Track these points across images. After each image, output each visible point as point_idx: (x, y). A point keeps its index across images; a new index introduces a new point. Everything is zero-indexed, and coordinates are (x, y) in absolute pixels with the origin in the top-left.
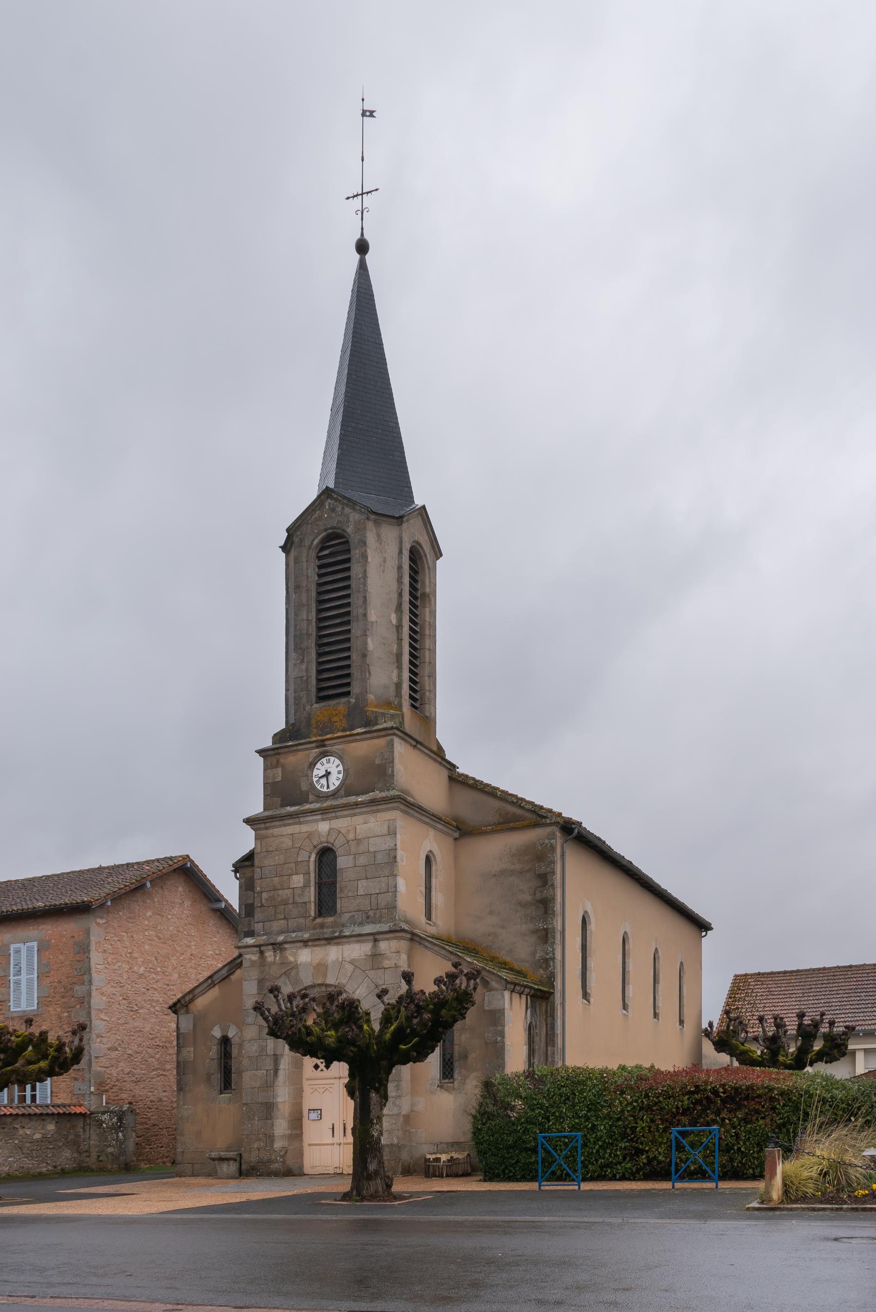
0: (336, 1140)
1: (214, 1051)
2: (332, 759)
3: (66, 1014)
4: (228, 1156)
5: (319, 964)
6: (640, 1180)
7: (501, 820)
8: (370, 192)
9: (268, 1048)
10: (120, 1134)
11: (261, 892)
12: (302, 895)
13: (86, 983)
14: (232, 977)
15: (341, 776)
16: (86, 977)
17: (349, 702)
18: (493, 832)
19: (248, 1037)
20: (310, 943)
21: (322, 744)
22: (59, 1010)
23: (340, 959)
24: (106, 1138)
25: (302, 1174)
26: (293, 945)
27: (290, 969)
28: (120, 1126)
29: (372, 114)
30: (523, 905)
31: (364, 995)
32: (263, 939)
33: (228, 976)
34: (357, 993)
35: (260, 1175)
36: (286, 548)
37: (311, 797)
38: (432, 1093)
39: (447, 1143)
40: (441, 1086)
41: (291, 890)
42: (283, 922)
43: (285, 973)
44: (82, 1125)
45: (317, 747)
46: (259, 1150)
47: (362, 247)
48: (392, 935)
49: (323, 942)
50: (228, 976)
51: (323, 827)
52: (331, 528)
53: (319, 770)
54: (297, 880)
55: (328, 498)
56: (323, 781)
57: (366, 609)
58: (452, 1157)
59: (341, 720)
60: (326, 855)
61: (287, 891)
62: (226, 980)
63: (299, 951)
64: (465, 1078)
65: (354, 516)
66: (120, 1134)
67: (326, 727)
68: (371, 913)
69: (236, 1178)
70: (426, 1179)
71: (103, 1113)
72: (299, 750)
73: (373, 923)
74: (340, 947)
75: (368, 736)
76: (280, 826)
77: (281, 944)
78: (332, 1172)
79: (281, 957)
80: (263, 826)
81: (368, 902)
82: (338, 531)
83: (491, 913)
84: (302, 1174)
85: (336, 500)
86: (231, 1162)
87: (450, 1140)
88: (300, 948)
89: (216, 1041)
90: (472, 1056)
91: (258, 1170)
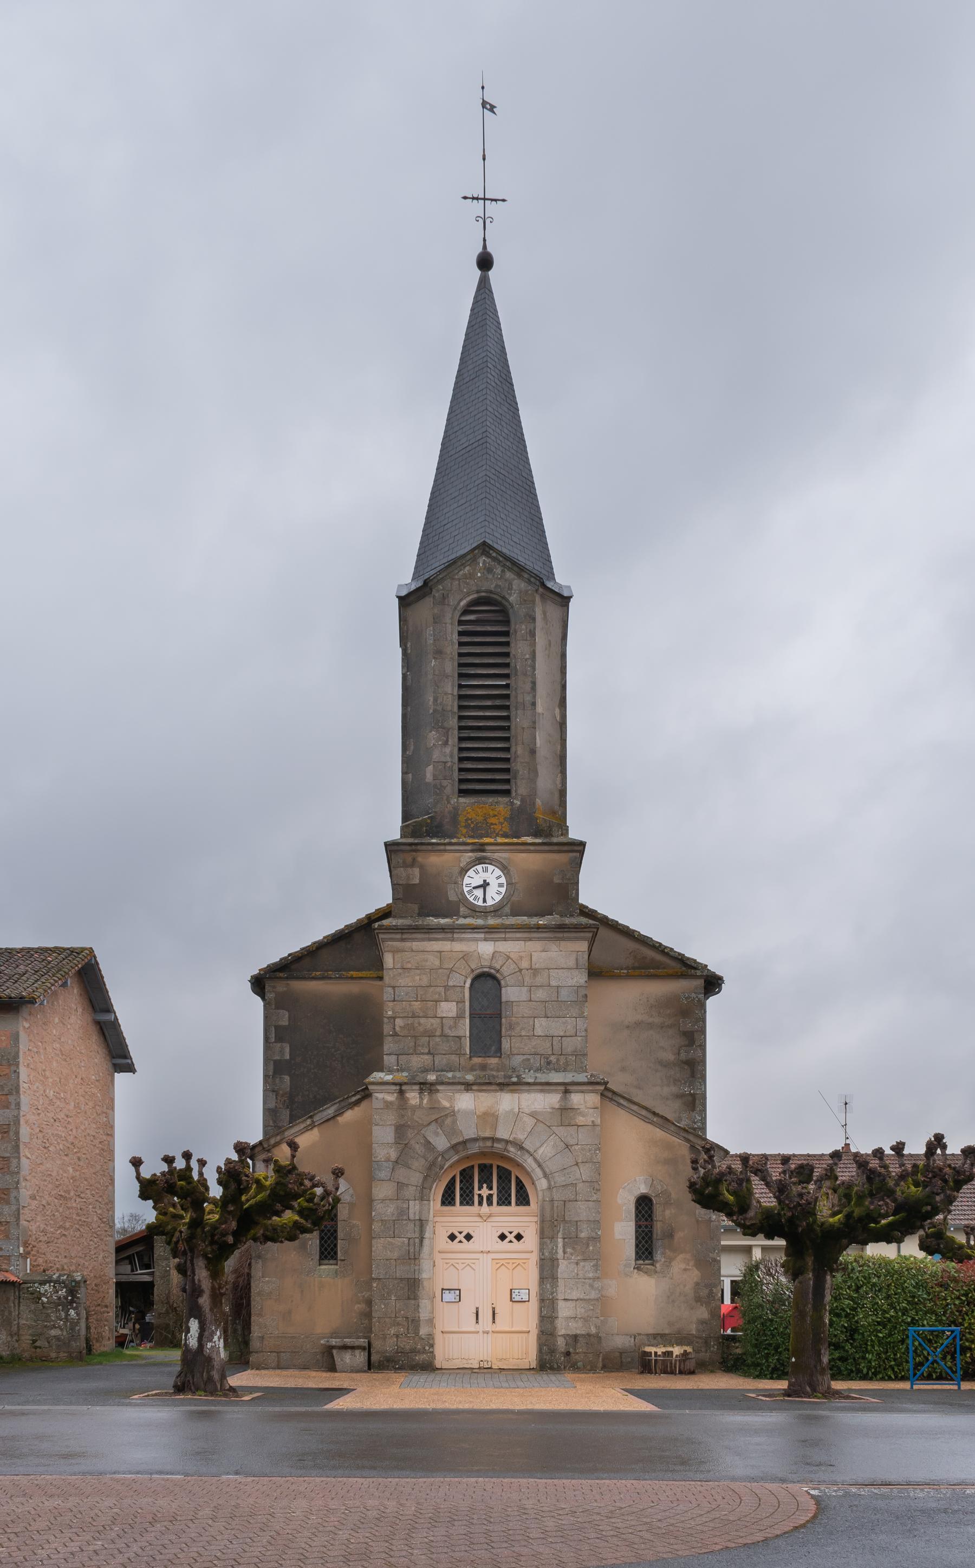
2: (491, 868)
4: (357, 1344)
5: (485, 1114)
7: (636, 964)
8: (496, 200)
10: (72, 1312)
11: (394, 1018)
12: (455, 1026)
13: (13, 1107)
14: (339, 1119)
15: (503, 890)
16: (11, 1099)
17: (512, 803)
18: (629, 977)
19: (381, 1196)
20: (475, 1087)
21: (481, 848)
23: (517, 1110)
24: (48, 1315)
25: (428, 1367)
27: (444, 1118)
28: (72, 1302)
29: (492, 109)
30: (665, 1064)
31: (550, 1155)
32: (403, 1076)
33: (334, 1117)
34: (540, 1151)
35: (399, 1369)
36: (405, 602)
37: (463, 910)
38: (627, 1275)
39: (648, 1335)
40: (638, 1268)
41: (438, 1020)
42: (426, 1057)
43: (436, 1120)
44: (564, 1310)
45: (472, 851)
46: (397, 1336)
47: (485, 262)
48: (590, 1088)
49: (493, 1087)
50: (334, 1117)
52: (486, 591)
53: (473, 878)
54: (448, 1009)
55: (482, 554)
56: (479, 893)
57: (534, 697)
58: (685, 1351)
59: (502, 824)
60: (487, 981)
61: (432, 1020)
62: (331, 1122)
63: (457, 1096)
64: (670, 1261)
65: (519, 585)
66: (72, 1312)
67: (479, 829)
68: (553, 1058)
69: (365, 1372)
71: (43, 1283)
72: (445, 851)
74: (516, 1095)
75: (546, 848)
76: (423, 940)
77: (432, 1084)
79: (430, 1100)
80: (399, 936)
81: (549, 1045)
82: (495, 596)
83: (623, 1069)
84: (428, 1367)
85: (494, 559)
86: (357, 1352)
87: (651, 1331)
88: (459, 1091)
90: (679, 1235)
91: (396, 1362)
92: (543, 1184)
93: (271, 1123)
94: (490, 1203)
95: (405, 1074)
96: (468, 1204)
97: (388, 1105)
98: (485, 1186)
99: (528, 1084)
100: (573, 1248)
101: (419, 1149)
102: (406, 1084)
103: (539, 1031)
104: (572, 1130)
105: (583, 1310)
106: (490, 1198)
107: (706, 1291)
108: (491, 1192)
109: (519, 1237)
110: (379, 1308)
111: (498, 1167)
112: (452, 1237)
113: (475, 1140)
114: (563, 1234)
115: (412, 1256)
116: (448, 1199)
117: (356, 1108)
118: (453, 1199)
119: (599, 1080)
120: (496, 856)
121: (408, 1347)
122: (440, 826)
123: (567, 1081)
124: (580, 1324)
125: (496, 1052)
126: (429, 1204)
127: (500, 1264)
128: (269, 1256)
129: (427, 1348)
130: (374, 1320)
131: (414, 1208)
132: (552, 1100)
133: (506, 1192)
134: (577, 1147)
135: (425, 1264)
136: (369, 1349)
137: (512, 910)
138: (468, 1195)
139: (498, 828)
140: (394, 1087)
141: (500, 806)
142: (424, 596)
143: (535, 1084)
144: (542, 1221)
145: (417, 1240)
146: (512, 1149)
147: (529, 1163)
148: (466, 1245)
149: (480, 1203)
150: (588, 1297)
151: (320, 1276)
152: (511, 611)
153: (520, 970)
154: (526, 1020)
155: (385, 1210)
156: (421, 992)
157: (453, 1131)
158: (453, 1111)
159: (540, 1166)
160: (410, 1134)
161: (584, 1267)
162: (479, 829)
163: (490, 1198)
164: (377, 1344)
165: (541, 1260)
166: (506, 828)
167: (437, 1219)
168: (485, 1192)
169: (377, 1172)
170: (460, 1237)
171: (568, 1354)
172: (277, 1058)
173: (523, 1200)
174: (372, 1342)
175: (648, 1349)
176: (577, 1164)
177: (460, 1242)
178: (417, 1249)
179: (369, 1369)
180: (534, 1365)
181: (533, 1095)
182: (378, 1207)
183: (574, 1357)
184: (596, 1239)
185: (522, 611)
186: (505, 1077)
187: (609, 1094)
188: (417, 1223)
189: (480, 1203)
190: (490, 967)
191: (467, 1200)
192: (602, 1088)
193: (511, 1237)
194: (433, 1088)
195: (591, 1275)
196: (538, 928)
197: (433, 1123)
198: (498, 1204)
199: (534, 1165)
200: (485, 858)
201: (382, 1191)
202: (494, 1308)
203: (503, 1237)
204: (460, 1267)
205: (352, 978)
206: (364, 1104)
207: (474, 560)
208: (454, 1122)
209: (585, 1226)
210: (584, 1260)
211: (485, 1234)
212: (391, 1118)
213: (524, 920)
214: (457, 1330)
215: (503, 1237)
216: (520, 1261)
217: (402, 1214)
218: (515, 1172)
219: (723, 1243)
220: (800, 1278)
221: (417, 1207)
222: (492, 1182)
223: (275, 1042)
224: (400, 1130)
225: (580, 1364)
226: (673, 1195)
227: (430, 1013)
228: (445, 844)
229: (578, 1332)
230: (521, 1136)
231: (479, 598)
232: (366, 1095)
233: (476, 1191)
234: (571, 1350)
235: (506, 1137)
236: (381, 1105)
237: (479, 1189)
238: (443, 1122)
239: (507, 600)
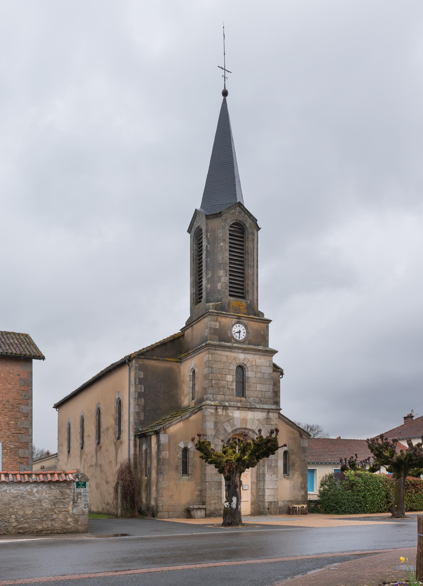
1: (180, 455)
2: (241, 326)
3: (13, 422)
5: (243, 419)
6: (387, 512)
8: (228, 72)
11: (212, 380)
15: (245, 334)
16: (29, 401)
20: (241, 409)
22: (7, 419)
26: (233, 408)
27: (230, 420)
32: (217, 403)
35: (216, 516)
39: (287, 501)
42: (222, 396)
45: (236, 318)
46: (215, 504)
47: (225, 93)
48: (276, 411)
51: (242, 356)
56: (237, 334)
60: (241, 368)
61: (224, 382)
62: (187, 420)
63: (234, 411)
68: (262, 399)
70: (287, 515)
72: (228, 317)
75: (260, 321)
76: (221, 350)
77: (227, 407)
79: (226, 413)
80: (214, 348)
85: (242, 209)
86: (202, 510)
87: (288, 500)
88: (235, 410)
89: (181, 450)
90: (296, 465)
93: (137, 418)
97: (212, 414)
99: (258, 408)
100: (270, 470)
101: (222, 431)
102: (219, 406)
103: (258, 389)
107: (304, 485)
113: (239, 429)
120: (243, 321)
121: (218, 508)
122: (224, 307)
124: (272, 498)
128: (165, 473)
137: (248, 342)
139: (243, 310)
140: (214, 407)
141: (243, 303)
142: (217, 217)
146: (250, 432)
151: (183, 481)
152: (246, 230)
153: (252, 365)
154: (254, 384)
156: (221, 371)
157: (233, 425)
160: (219, 425)
162: (237, 310)
166: (245, 311)
171: (269, 509)
172: (139, 391)
175: (295, 506)
183: (271, 510)
185: (250, 231)
190: (243, 363)
195: (275, 480)
196: (259, 350)
200: (240, 322)
205: (167, 361)
207: (236, 208)
208: (233, 421)
210: (273, 474)
212: (212, 419)
213: (252, 347)
219: (309, 468)
220: (399, 479)
223: (139, 384)
224: (216, 423)
225: (272, 512)
226: (295, 451)
227: (224, 379)
228: (228, 315)
229: (272, 501)
231: (236, 222)
235: (250, 428)
239: (245, 225)
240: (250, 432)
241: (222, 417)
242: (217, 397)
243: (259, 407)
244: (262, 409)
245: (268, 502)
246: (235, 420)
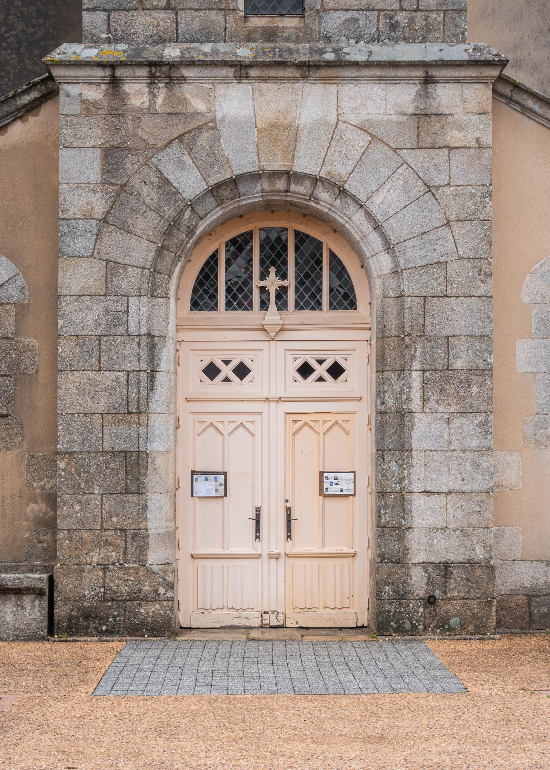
0: (263, 548)
4: (26, 583)
5: (274, 125)
9: (133, 318)
19: (75, 288)
20: (254, 72)
23: (333, 118)
25: (165, 629)
26: (207, 72)
27: (193, 133)
31: (396, 206)
32: (118, 51)
34: (378, 199)
35: (108, 632)
42: (162, 15)
43: (180, 138)
44: (424, 514)
46: (105, 568)
48: (473, 73)
49: (290, 72)
63: (221, 89)
68: (402, 18)
69: (42, 639)
73: (406, 40)
74: (333, 88)
77: (173, 65)
78: (257, 623)
79: (170, 97)
84: (165, 629)
86: (27, 600)
88: (224, 80)
91: (102, 619)
92: (382, 263)
94: (282, 305)
95: (122, 47)
96: (240, 306)
97: (89, 108)
98: (272, 270)
99: (356, 64)
100: (442, 390)
101: (149, 195)
102: (123, 64)
104: (439, 156)
105: (460, 514)
106: (281, 293)
108: (284, 283)
109: (336, 371)
110: (69, 512)
111: (297, 234)
112: (211, 371)
113: (255, 176)
114: (423, 363)
115: (134, 410)
116: (203, 297)
117: (32, 119)
118: (214, 297)
119: (489, 57)
121: (125, 589)
123: (429, 58)
124: (455, 540)
125: (294, 8)
126: (167, 304)
127: (299, 423)
129: (162, 590)
130: (60, 535)
131: (139, 311)
132: (403, 96)
133: (313, 283)
134: (447, 191)
135: (159, 423)
136: (49, 593)
138: (240, 290)
140: (100, 73)
143: (369, 65)
144: (382, 338)
145: (143, 376)
146: (323, 195)
147: (356, 223)
148: (238, 387)
149: (264, 305)
150: (468, 488)
155: (82, 317)
157: (214, 160)
158: (214, 120)
159: (377, 227)
160: (131, 164)
161: (461, 427)
163: (281, 293)
164: (66, 584)
165: (380, 413)
167: (182, 336)
168: (273, 283)
169: (68, 241)
170: (227, 371)
171: (431, 601)
173: (345, 299)
174: (57, 579)
176: (448, 224)
177: (227, 380)
178: (144, 392)
179: (51, 632)
180: (364, 620)
181: (364, 87)
182: (69, 309)
183: (443, 607)
184: (484, 372)
186: (312, 51)
187: (508, 92)
188: (144, 341)
189: (264, 305)
191: (239, 298)
192: (495, 73)
193: (321, 370)
194: (175, 74)
195: (475, 444)
197: (175, 145)
198: (298, 306)
199: (367, 227)
201: (78, 277)
202: (289, 509)
203: (305, 370)
204: (226, 428)
206: (45, 110)
208: (215, 141)
209: (463, 346)
210: (462, 413)
211: (273, 367)
212: (95, 133)
214: (219, 551)
215: (305, 370)
216: (338, 418)
217: (116, 321)
218: (330, 244)
221: (144, 310)
222: (285, 263)
224: (112, 157)
225: (454, 621)
229: (451, 557)
230: (340, 169)
232: (50, 92)
233: (257, 282)
234: (438, 593)
236: (75, 108)
237: (263, 277)
238: (194, 140)
240: (323, 195)
241: (147, 124)
242: (129, 24)
243: (361, 58)
244: (380, 65)
245: (425, 565)
246: (224, 131)
